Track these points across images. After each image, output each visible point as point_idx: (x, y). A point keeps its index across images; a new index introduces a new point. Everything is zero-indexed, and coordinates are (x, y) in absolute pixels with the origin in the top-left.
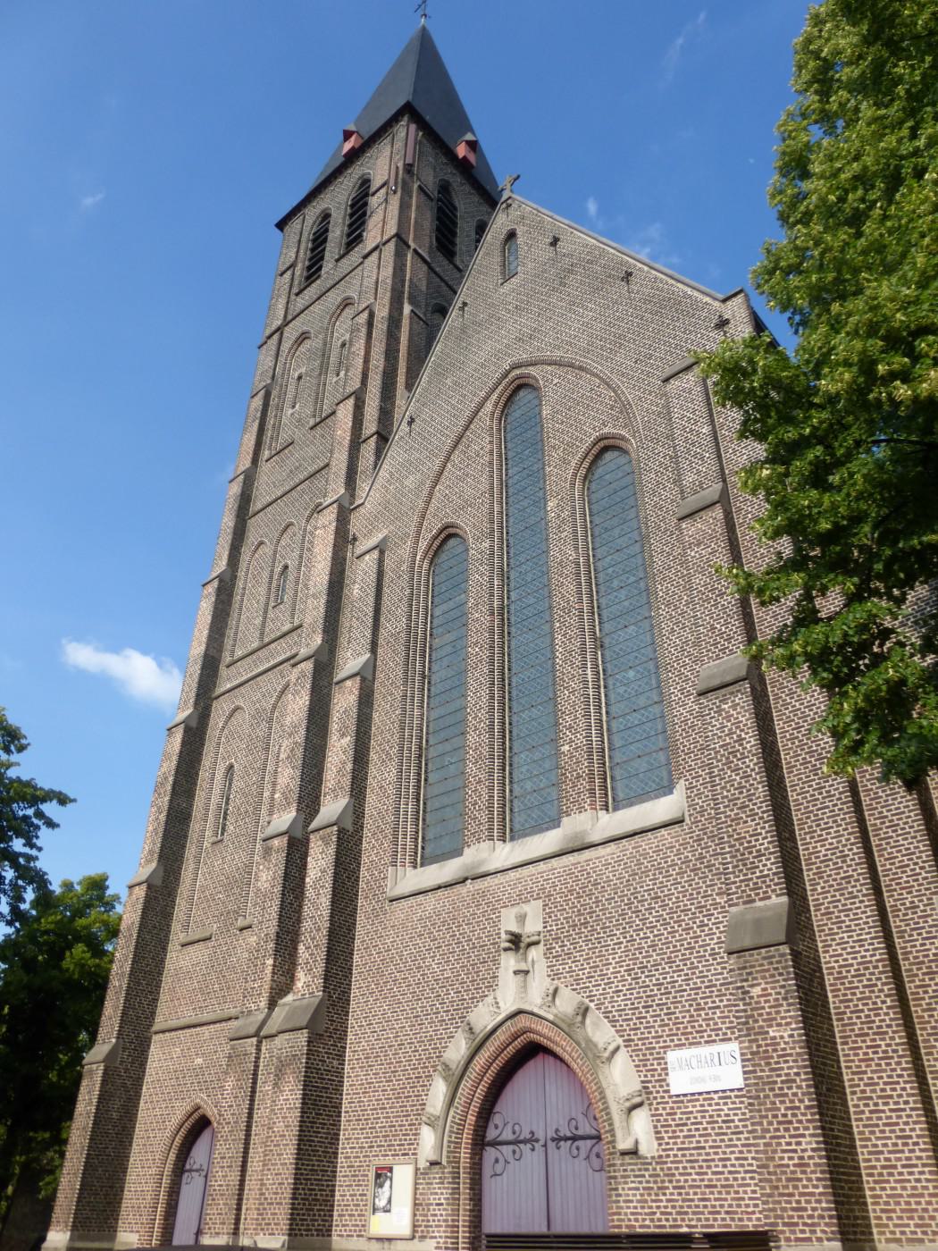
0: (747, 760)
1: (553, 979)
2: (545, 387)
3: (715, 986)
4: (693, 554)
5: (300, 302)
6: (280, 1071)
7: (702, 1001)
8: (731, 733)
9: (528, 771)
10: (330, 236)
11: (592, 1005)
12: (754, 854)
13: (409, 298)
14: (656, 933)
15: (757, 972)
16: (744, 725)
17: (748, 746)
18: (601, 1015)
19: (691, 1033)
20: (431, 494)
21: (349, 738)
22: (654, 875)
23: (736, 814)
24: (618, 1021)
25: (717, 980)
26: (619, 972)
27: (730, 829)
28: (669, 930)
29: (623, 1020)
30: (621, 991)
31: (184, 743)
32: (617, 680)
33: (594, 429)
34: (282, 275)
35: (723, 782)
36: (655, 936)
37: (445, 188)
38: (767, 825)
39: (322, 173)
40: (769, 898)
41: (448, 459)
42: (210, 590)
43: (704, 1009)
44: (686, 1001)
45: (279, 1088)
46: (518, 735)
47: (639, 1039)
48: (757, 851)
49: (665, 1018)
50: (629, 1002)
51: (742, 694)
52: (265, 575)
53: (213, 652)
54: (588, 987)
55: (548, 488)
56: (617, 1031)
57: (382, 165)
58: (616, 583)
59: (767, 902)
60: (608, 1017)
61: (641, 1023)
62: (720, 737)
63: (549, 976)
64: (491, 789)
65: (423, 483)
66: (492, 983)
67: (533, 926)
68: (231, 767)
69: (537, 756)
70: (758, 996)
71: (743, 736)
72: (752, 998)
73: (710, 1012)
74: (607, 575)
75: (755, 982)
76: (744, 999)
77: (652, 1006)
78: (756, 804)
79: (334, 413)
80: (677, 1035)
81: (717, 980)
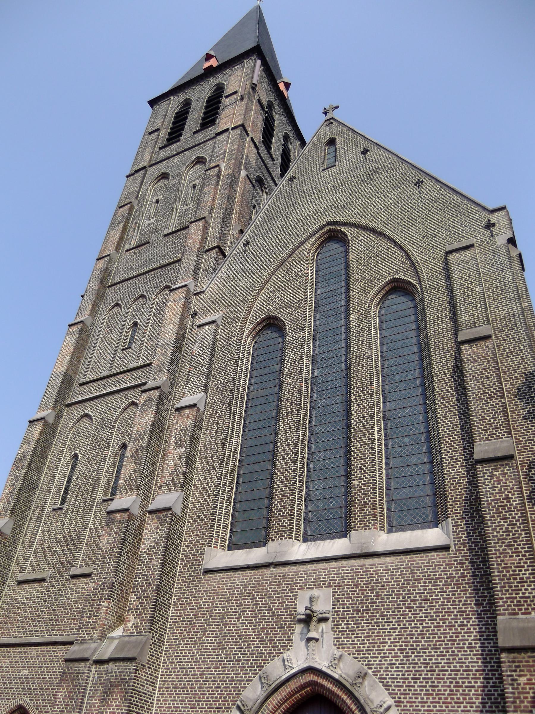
0: (513, 513)
1: (339, 648)
2: (352, 240)
3: (471, 671)
4: (470, 367)
5: (163, 154)
6: (109, 689)
7: (460, 681)
8: (500, 492)
9: (320, 494)
10: (190, 116)
11: (370, 671)
12: (518, 580)
13: (245, 167)
14: (424, 625)
15: (524, 666)
16: (511, 489)
17: (514, 503)
18: (377, 680)
19: (451, 703)
20: (258, 294)
21: (184, 449)
22: (425, 583)
23: (503, 550)
24: (391, 686)
25: (472, 666)
26: (394, 650)
27: (499, 560)
28: (435, 624)
29: (395, 686)
30: (394, 664)
31: (41, 433)
32: (395, 442)
33: (389, 274)
34: (150, 133)
35: (494, 525)
36: (423, 627)
37: (270, 105)
38: (528, 561)
39: (183, 77)
40: (530, 613)
41: (273, 273)
42: (75, 329)
43: (461, 687)
44: (448, 679)
45: (106, 702)
46: (314, 468)
47: (407, 702)
48: (520, 578)
49: (430, 689)
50: (401, 673)
51: (509, 467)
52: (118, 326)
53: (70, 373)
54: (367, 658)
55: (351, 306)
56: (390, 694)
57: (235, 80)
58: (397, 377)
59: (528, 616)
60: (383, 682)
61: (410, 690)
62: (492, 494)
63: (335, 645)
64: (293, 502)
65: (253, 285)
66: (287, 645)
67: (324, 604)
68: (76, 456)
69: (329, 484)
70: (525, 684)
71: (510, 496)
72: (519, 684)
73: (467, 689)
74: (391, 370)
75: (522, 673)
76: (513, 684)
77: (419, 679)
78: (519, 545)
79: (188, 227)
80: (439, 703)
81: (472, 666)
